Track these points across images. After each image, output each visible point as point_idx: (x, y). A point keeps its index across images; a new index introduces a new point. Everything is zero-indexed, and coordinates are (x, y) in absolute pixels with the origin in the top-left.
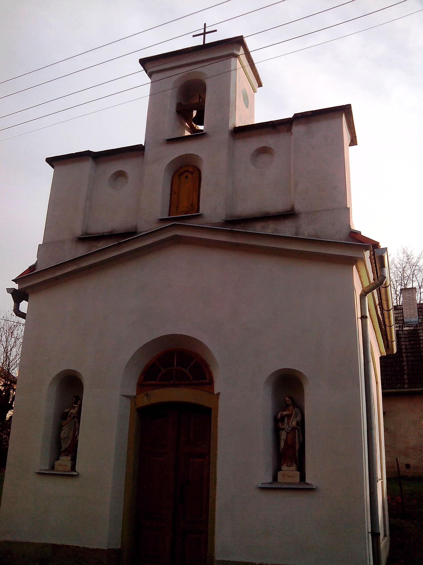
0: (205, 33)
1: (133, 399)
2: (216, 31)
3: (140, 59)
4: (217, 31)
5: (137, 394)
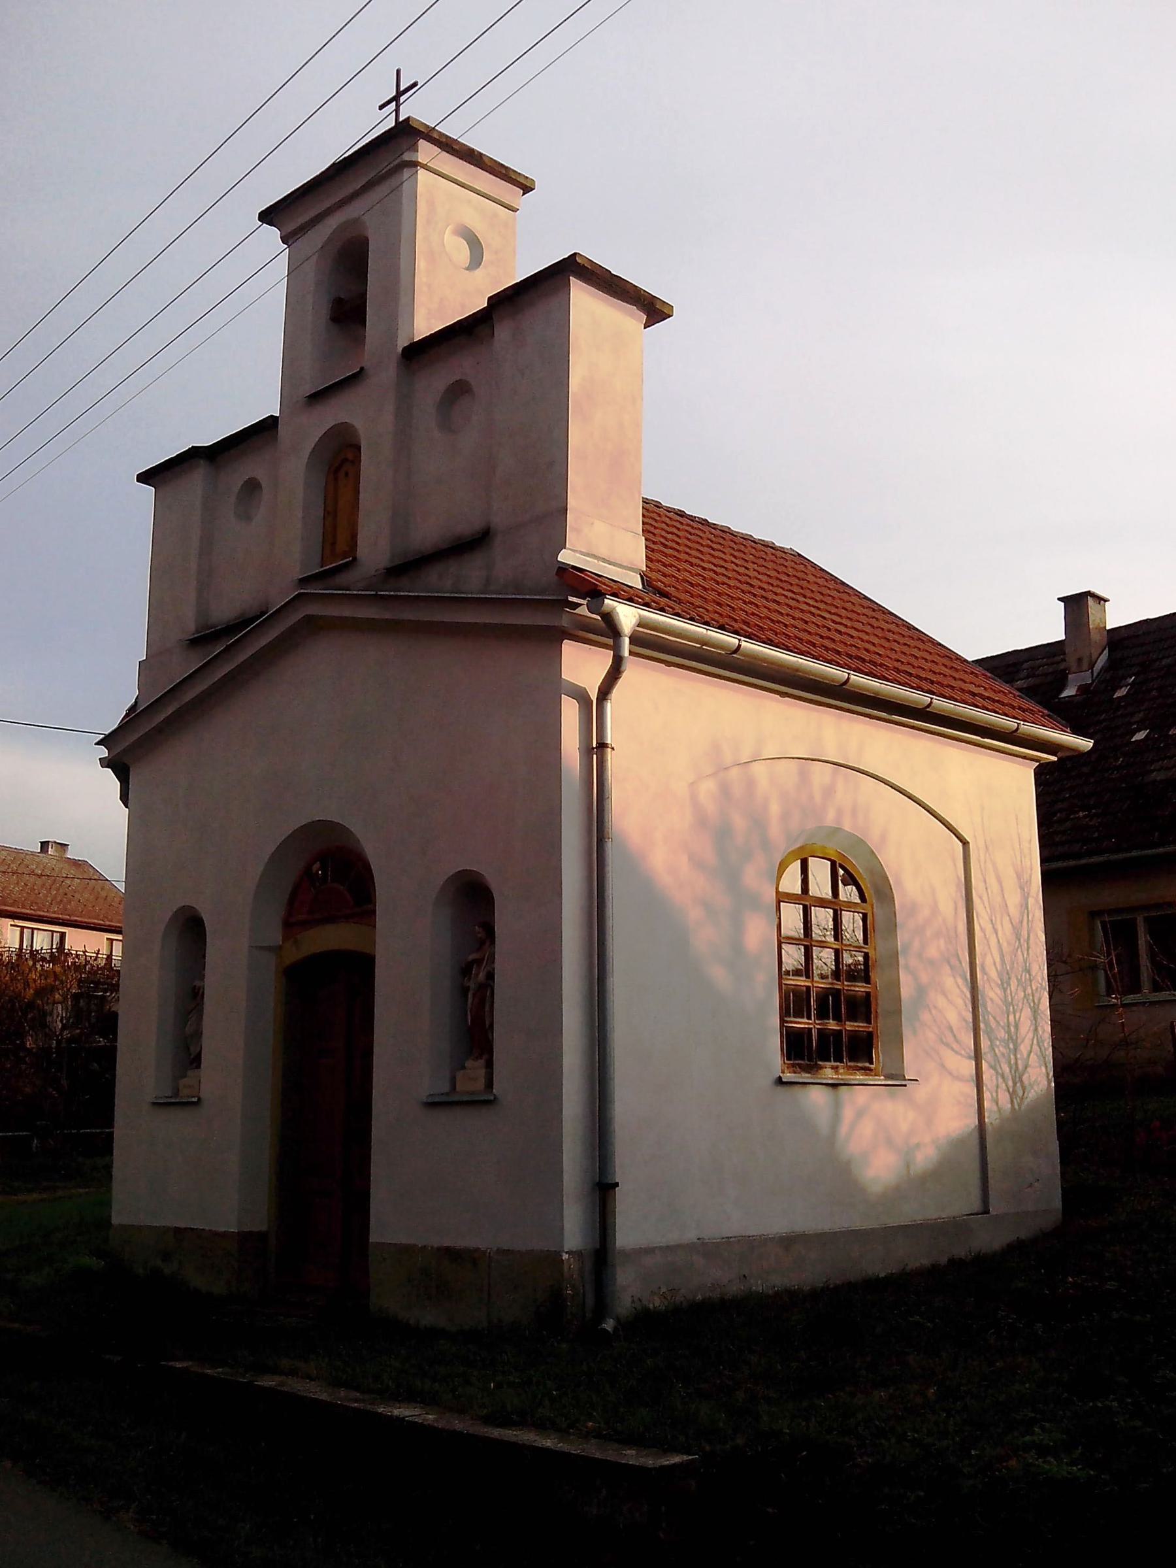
0: (396, 99)
1: (277, 950)
2: (398, 72)
3: (138, 481)
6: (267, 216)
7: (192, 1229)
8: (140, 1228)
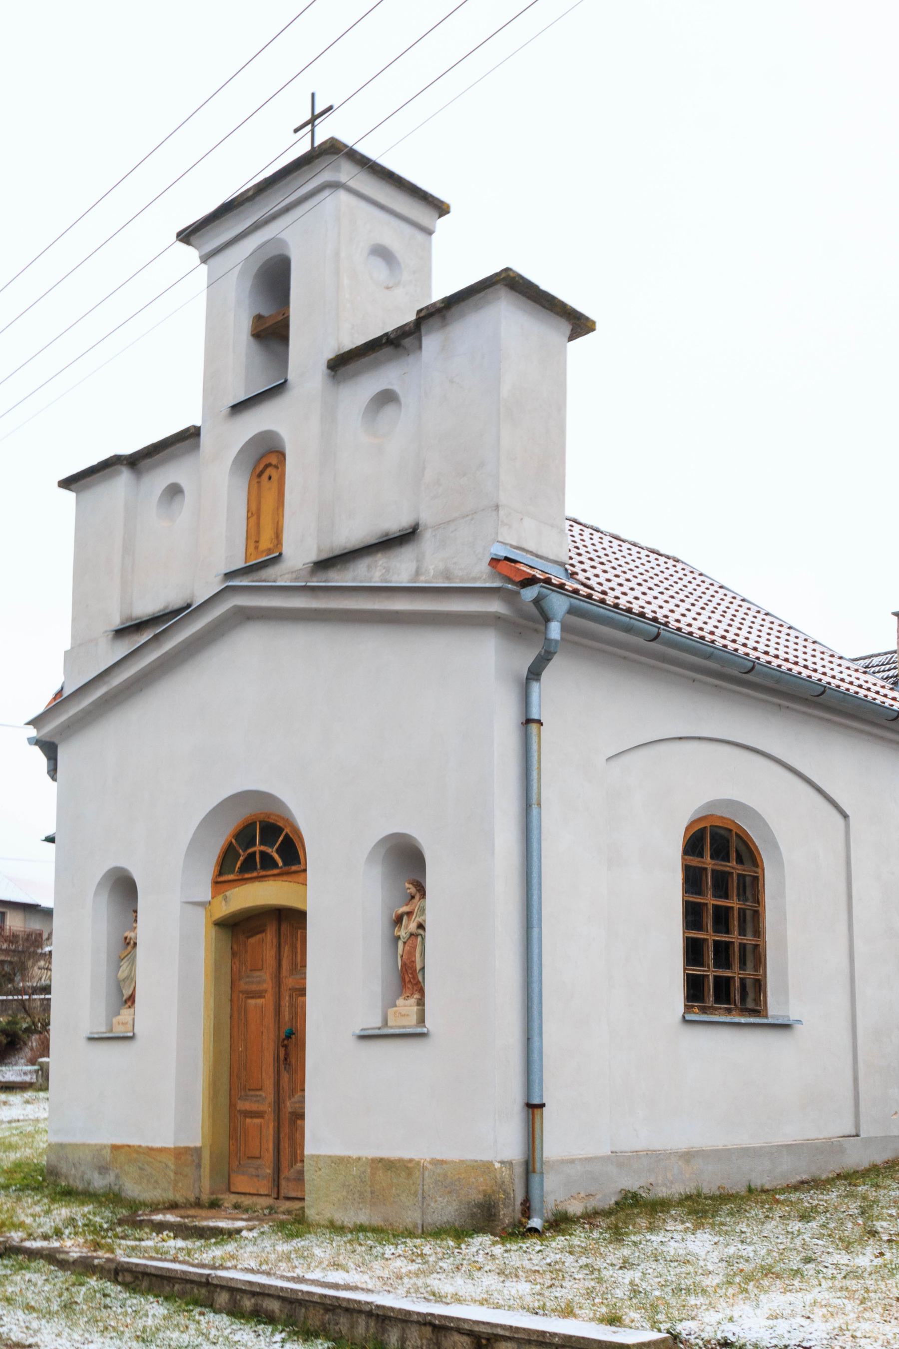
0: (312, 121)
2: (313, 95)
4: (292, 131)
5: (213, 898)
6: (187, 236)
7: (129, 1146)
8: (76, 1146)
